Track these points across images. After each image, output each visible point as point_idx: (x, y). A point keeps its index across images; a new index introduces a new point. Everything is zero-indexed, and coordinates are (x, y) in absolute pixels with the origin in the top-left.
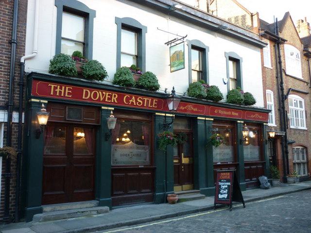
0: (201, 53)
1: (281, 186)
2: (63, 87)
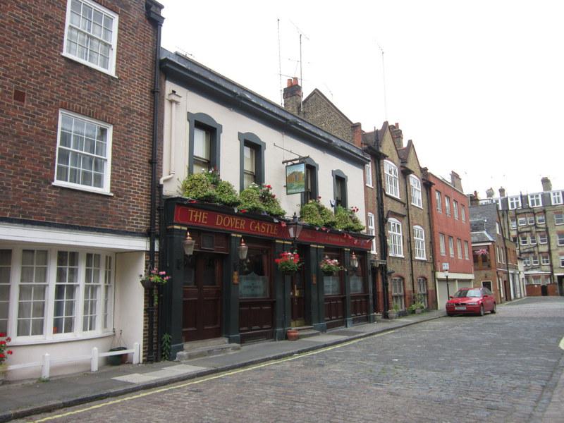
0: (309, 171)
1: (383, 322)
2: (201, 213)
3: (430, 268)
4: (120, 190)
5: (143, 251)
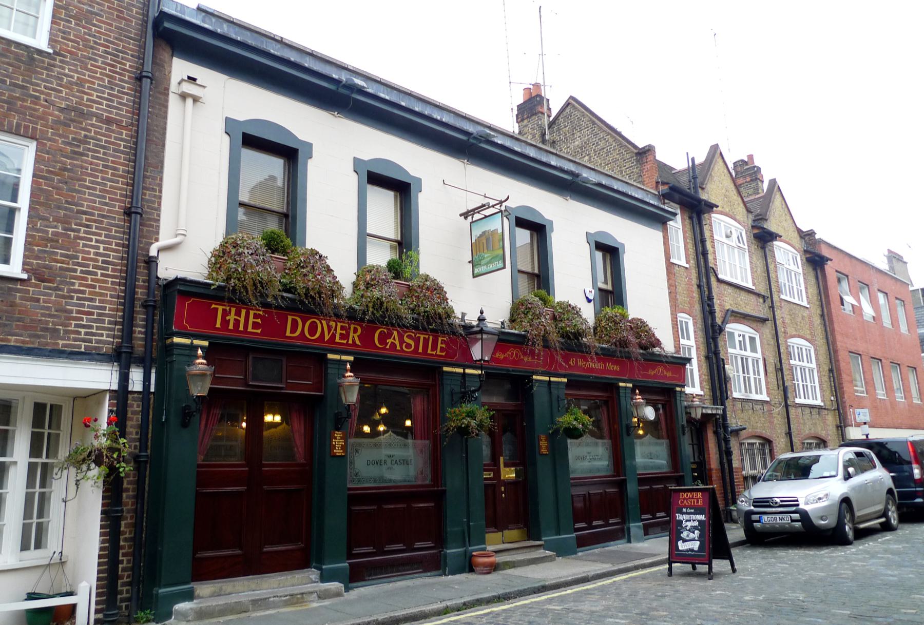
2: (243, 312)
3: (831, 420)
4: (46, 267)
5: (107, 390)
